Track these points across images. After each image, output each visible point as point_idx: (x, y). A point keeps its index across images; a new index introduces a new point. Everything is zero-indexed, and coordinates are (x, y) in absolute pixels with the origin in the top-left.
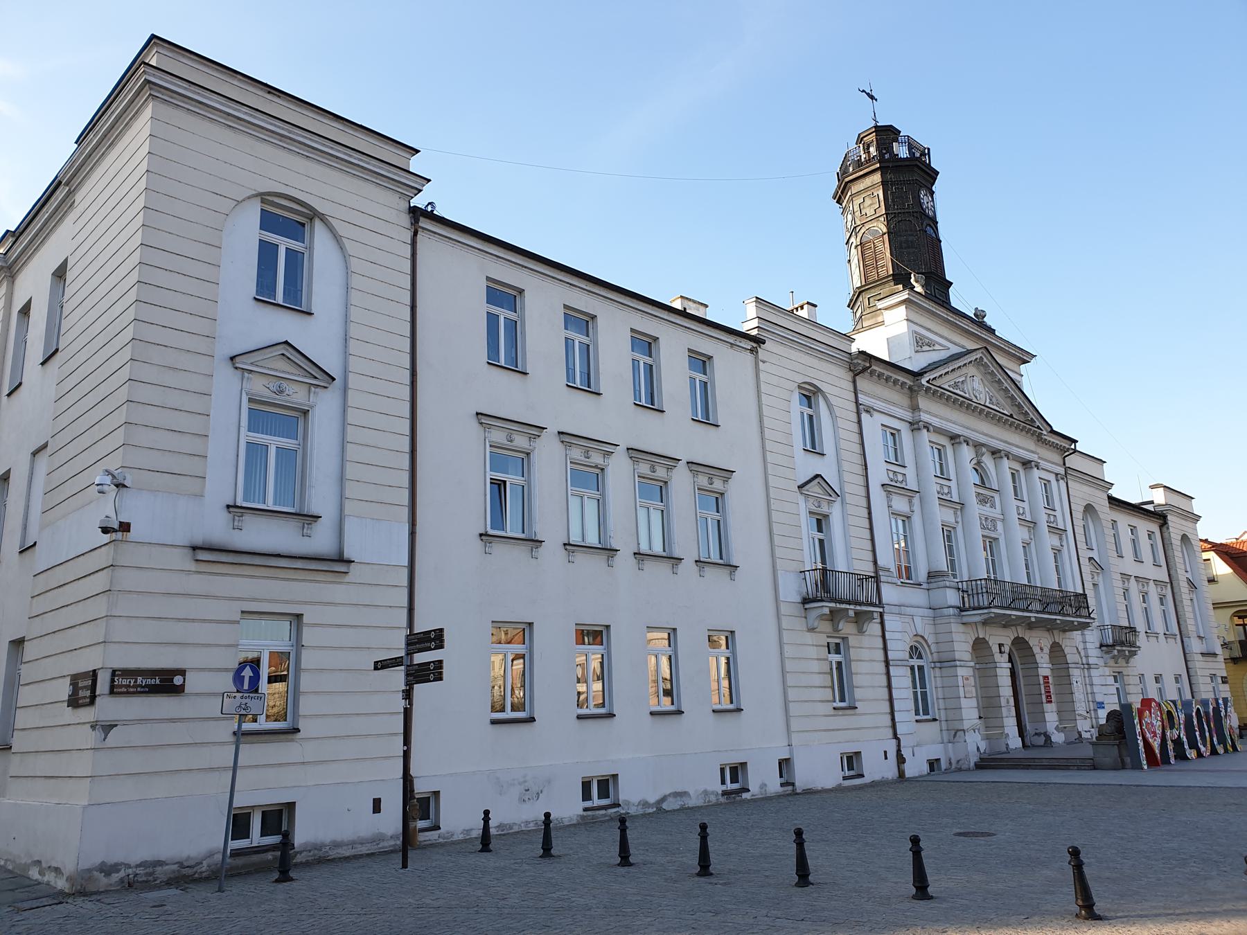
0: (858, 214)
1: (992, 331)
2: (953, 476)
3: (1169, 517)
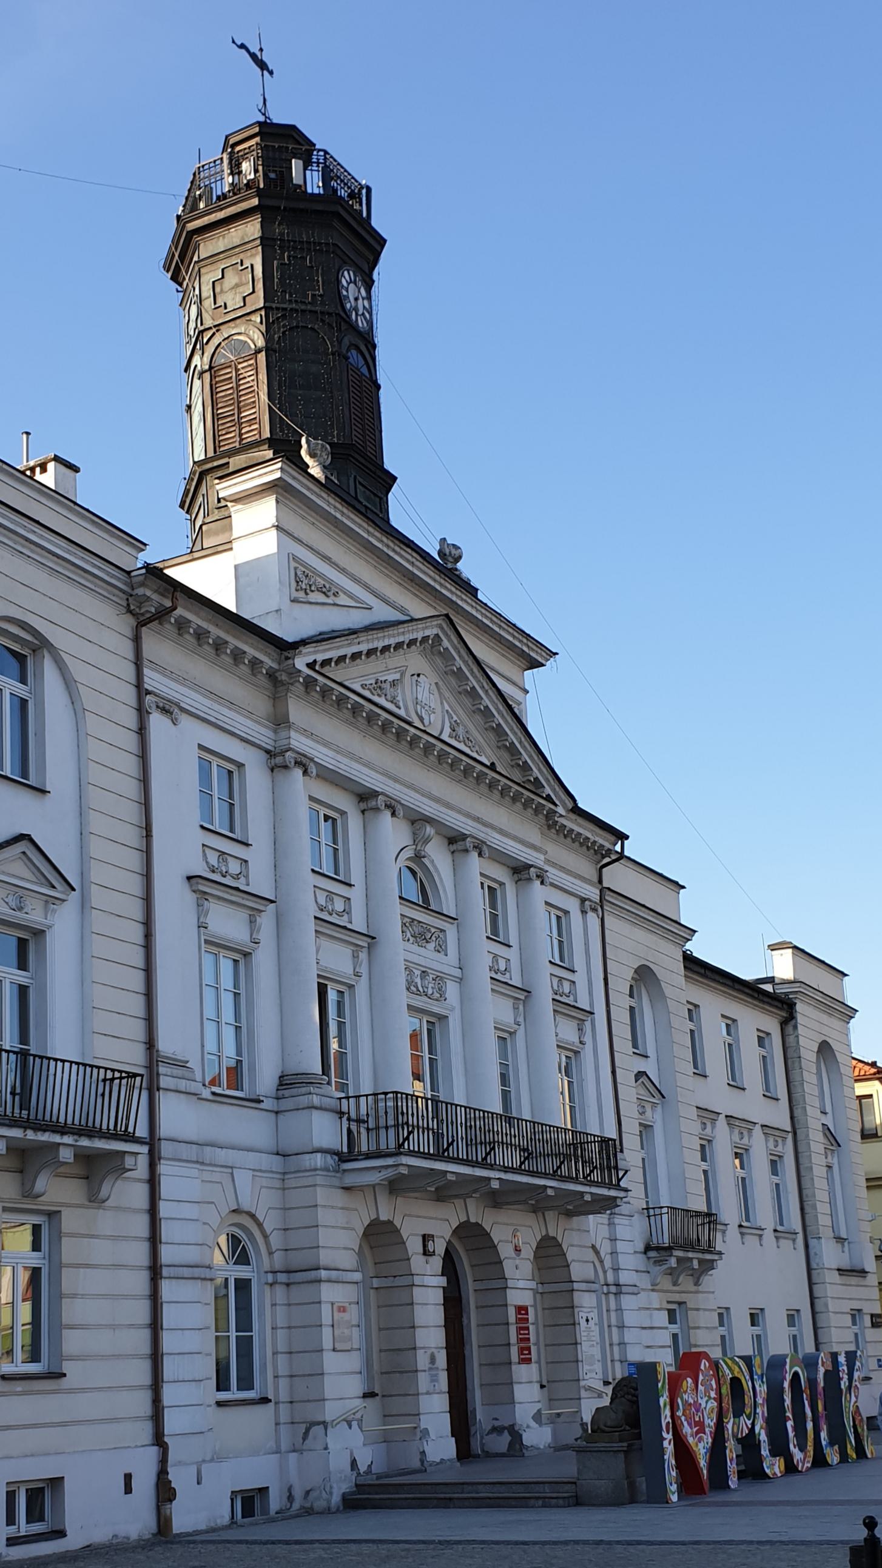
0: (208, 303)
1: (473, 591)
2: (357, 876)
3: (800, 1007)
